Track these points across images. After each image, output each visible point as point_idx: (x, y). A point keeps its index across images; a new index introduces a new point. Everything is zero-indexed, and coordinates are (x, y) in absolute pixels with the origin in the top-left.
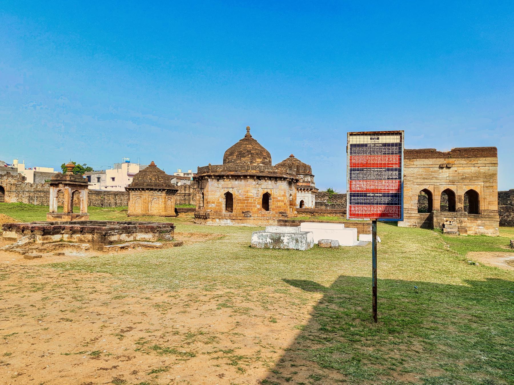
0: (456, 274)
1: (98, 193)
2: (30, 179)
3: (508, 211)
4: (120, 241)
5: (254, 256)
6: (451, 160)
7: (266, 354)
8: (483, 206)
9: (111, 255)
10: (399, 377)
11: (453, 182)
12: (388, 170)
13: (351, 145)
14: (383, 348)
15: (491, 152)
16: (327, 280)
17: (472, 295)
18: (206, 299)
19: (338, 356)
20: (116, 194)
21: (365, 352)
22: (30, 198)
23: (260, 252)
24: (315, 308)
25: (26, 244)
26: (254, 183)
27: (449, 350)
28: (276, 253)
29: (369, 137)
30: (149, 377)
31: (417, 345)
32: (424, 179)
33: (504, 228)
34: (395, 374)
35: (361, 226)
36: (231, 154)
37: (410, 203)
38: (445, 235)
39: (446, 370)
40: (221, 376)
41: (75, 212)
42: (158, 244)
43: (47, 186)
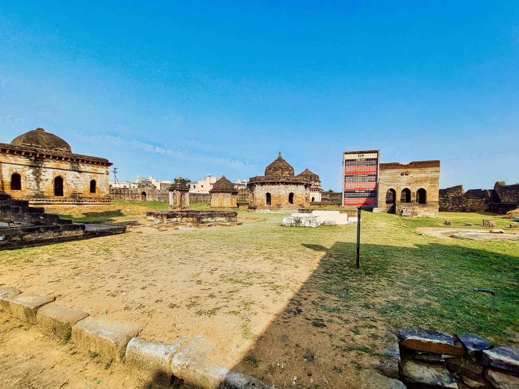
0: (408, 239)
1: (194, 195)
2: (158, 188)
3: (445, 202)
4: (208, 222)
5: (285, 231)
6: (409, 170)
7: (292, 285)
8: (429, 198)
9: (203, 229)
10: (371, 299)
11: (409, 184)
12: (369, 176)
13: (346, 160)
14: (362, 283)
15: (436, 164)
16: (328, 244)
17: (419, 253)
18: (256, 254)
19: (335, 287)
20: (204, 195)
21: (351, 285)
22: (159, 198)
23: (287, 229)
24: (321, 260)
25: (159, 223)
26: (284, 187)
27: (403, 285)
28: (297, 229)
29: (357, 155)
30: (228, 295)
31: (384, 282)
32: (391, 182)
33: (442, 213)
34: (369, 298)
35: (350, 212)
36: (270, 169)
37: (382, 197)
38: (403, 217)
39: (401, 296)
40: (268, 296)
41: (183, 206)
42: (228, 224)
43: (167, 192)
